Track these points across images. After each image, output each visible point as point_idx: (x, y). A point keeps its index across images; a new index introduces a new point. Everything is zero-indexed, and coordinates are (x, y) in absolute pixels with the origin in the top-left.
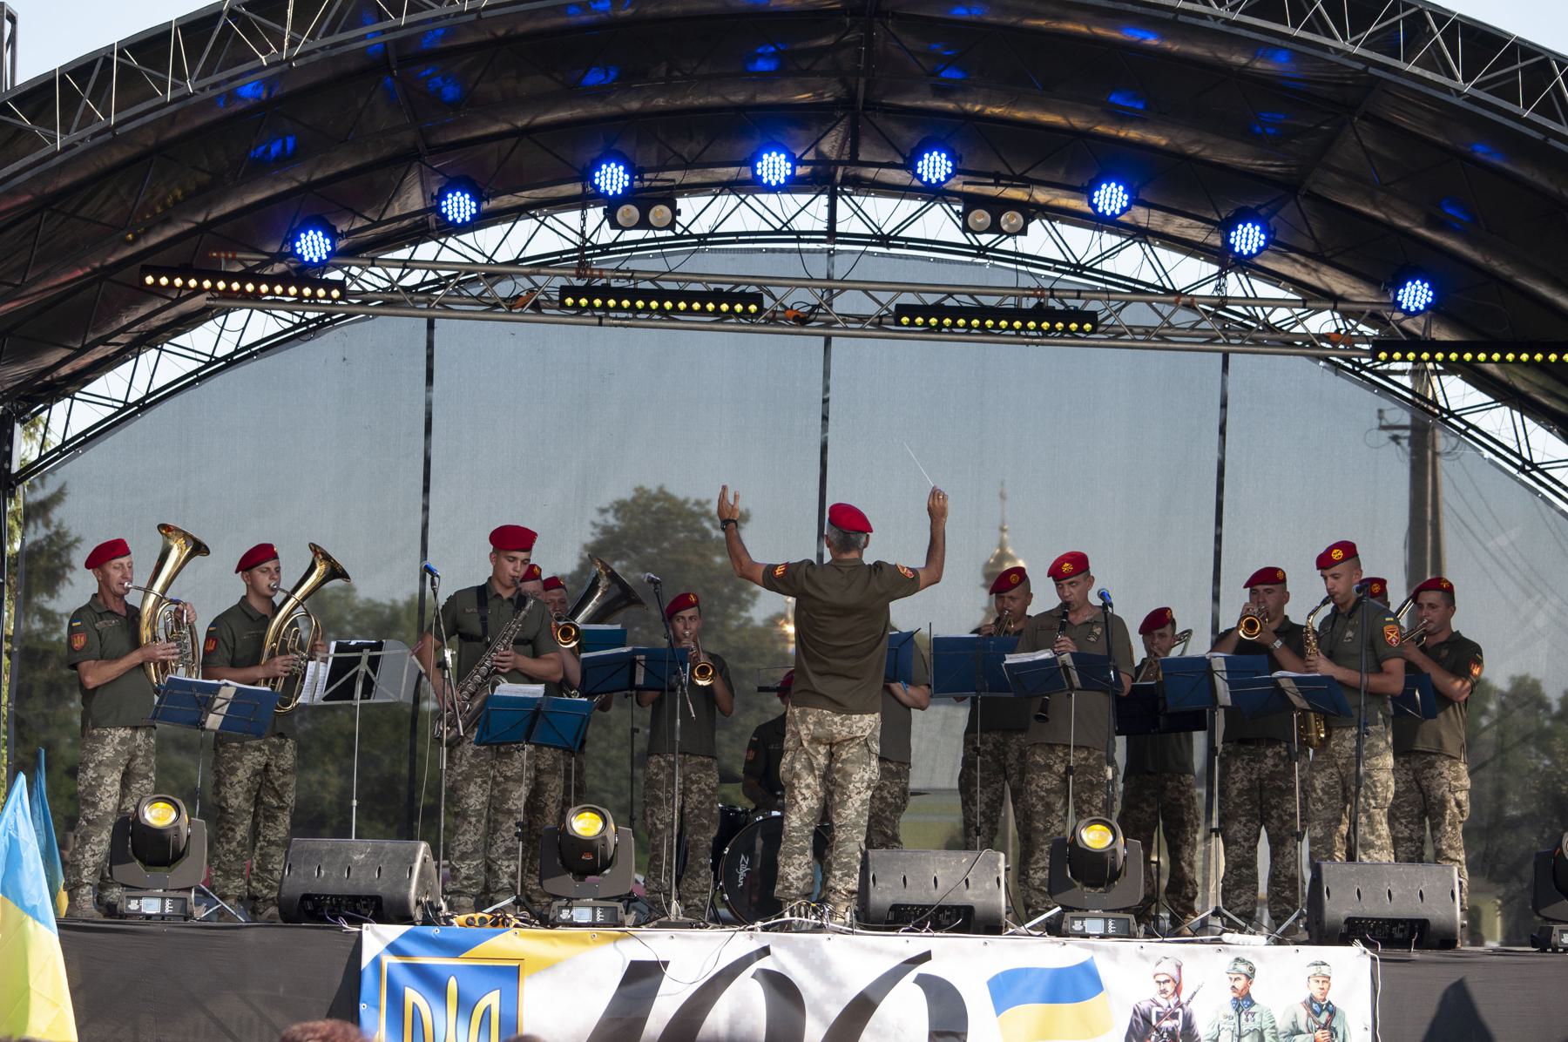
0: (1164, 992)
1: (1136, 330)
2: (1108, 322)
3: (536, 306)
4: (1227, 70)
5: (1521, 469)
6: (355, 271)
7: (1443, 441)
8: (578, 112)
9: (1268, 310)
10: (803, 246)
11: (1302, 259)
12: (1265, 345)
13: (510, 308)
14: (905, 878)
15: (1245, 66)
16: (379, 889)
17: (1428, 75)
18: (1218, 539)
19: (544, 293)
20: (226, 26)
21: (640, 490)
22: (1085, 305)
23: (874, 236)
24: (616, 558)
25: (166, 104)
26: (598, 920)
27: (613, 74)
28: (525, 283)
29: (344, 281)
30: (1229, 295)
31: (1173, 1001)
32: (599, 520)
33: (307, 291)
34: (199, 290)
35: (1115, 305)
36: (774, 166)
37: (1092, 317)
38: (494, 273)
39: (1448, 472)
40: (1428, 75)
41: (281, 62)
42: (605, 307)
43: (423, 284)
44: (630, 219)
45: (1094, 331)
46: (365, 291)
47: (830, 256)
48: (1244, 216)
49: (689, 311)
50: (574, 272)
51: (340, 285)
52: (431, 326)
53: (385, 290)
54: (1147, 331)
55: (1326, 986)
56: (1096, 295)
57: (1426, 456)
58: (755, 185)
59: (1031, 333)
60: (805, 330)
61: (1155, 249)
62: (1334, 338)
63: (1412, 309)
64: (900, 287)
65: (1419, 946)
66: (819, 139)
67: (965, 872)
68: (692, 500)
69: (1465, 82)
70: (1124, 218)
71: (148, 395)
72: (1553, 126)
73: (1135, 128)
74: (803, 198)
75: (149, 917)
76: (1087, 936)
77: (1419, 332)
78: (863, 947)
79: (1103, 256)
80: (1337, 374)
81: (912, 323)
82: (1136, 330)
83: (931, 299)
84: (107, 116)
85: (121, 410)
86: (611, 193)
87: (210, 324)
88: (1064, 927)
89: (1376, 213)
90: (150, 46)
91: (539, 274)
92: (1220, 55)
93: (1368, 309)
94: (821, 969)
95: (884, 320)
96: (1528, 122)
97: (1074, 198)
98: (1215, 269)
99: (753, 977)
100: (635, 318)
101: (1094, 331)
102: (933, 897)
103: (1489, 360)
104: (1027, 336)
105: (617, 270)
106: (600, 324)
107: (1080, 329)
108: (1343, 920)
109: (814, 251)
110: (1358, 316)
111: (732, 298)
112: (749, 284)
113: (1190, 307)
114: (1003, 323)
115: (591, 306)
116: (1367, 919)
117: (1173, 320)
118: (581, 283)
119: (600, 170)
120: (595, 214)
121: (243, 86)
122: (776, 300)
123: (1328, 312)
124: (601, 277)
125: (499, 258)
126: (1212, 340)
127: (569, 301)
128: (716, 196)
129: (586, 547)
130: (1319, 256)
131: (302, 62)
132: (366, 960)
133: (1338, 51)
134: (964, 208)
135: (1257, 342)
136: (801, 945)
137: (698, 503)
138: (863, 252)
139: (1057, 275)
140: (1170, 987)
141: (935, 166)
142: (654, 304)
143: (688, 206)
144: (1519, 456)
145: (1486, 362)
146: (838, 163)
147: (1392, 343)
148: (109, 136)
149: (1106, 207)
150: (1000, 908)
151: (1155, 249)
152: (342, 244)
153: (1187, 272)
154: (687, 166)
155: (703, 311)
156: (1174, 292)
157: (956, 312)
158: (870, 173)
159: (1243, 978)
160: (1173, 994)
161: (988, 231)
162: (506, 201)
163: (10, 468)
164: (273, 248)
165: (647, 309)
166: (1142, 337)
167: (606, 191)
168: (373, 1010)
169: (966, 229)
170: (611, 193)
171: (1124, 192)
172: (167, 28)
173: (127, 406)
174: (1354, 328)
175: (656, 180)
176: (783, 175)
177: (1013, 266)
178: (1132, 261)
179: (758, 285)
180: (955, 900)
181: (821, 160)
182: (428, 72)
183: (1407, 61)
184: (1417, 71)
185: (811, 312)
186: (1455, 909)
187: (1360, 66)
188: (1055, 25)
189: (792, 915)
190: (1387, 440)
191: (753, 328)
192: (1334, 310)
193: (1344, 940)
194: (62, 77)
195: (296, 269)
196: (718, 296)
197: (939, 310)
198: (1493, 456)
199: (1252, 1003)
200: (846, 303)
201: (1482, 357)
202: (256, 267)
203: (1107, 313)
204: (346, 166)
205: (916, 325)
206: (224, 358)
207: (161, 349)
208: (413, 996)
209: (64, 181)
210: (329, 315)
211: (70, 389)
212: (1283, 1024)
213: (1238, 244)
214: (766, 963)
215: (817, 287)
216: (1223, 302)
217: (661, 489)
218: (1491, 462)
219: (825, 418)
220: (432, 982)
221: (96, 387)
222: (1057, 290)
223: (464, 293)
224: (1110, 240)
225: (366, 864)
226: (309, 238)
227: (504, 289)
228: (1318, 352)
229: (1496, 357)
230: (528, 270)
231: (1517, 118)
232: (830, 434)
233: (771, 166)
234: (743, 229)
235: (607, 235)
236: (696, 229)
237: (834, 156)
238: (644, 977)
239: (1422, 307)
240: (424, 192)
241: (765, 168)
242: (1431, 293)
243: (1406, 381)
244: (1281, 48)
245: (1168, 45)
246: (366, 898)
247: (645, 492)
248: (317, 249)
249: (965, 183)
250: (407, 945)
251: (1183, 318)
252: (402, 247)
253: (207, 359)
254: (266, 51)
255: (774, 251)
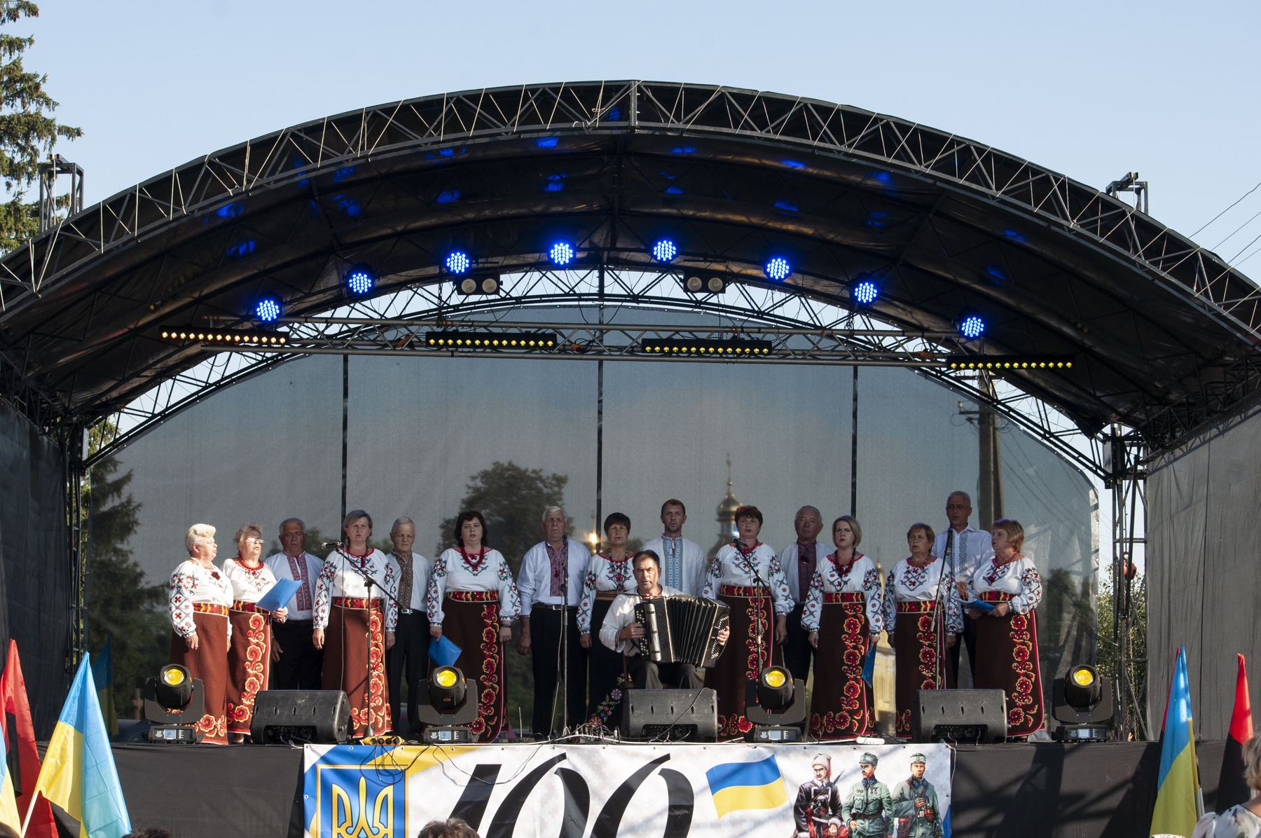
0: (819, 776)
1: (797, 352)
2: (779, 347)
3: (411, 345)
4: (850, 187)
5: (1044, 437)
6: (296, 325)
7: (999, 422)
8: (433, 221)
9: (881, 338)
10: (581, 303)
11: (902, 306)
12: (880, 361)
13: (395, 347)
14: (672, 708)
15: (860, 183)
16: (314, 722)
17: (974, 186)
18: (854, 485)
19: (416, 337)
20: (207, 172)
21: (497, 464)
22: (763, 337)
23: (629, 295)
24: (484, 508)
25: (169, 222)
26: (455, 738)
27: (456, 195)
28: (404, 331)
29: (289, 333)
30: (855, 328)
31: (826, 781)
32: (471, 484)
33: (264, 339)
34: (196, 341)
35: (782, 337)
36: (562, 252)
37: (768, 344)
38: (386, 324)
39: (1004, 440)
40: (974, 186)
41: (242, 193)
42: (455, 345)
43: (340, 333)
44: (471, 288)
45: (769, 353)
46: (301, 339)
47: (601, 309)
48: (864, 278)
49: (509, 346)
50: (434, 323)
51: (285, 335)
52: (346, 360)
53: (315, 337)
54: (804, 353)
55: (922, 769)
56: (771, 330)
57: (989, 430)
58: (549, 265)
59: (729, 356)
60: (585, 357)
61: (809, 301)
62: (922, 355)
63: (971, 336)
64: (644, 328)
65: (982, 741)
66: (591, 234)
67: (691, 702)
68: (530, 470)
69: (997, 190)
70: (787, 281)
71: (167, 409)
72: (1053, 218)
73: (793, 224)
74: (582, 273)
75: (169, 742)
76: (770, 742)
77: (977, 351)
78: (625, 752)
79: (775, 306)
80: (926, 378)
81: (653, 351)
82: (797, 352)
83: (665, 335)
84: (132, 229)
85: (150, 419)
86: (457, 272)
87: (204, 363)
88: (755, 736)
89: (947, 275)
90: (159, 186)
91: (412, 325)
92: (844, 176)
93: (944, 336)
94: (598, 768)
95: (635, 349)
96: (1037, 215)
97: (756, 269)
98: (846, 312)
99: (556, 773)
100: (475, 351)
101: (769, 353)
102: (671, 719)
103: (1020, 367)
104: (727, 358)
105: (463, 321)
106: (452, 356)
107: (761, 352)
108: (933, 727)
109: (591, 306)
110: (938, 341)
111: (536, 337)
112: (548, 328)
113: (831, 337)
114: (711, 350)
115: (446, 344)
116: (949, 726)
117: (820, 346)
118: (440, 330)
119: (450, 257)
120: (448, 287)
121: (221, 208)
122: (565, 338)
123: (920, 339)
124: (452, 326)
125: (388, 315)
126: (845, 358)
127: (432, 341)
128: (527, 272)
129: (464, 502)
130: (913, 303)
131: (256, 192)
132: (307, 767)
133: (917, 172)
134: (685, 277)
135: (875, 359)
136: (586, 752)
137: (534, 471)
138: (621, 306)
139: (746, 318)
140: (823, 773)
141: (665, 250)
142: (487, 342)
143: (508, 280)
144: (1042, 428)
145: (1018, 368)
146: (604, 249)
147: (962, 356)
148: (134, 243)
149: (775, 274)
150: (714, 725)
151: (809, 301)
152: (288, 309)
153: (829, 314)
154: (506, 253)
155: (518, 346)
156: (822, 328)
157: (680, 343)
158: (624, 255)
159: (870, 766)
160: (825, 777)
161: (701, 291)
162: (391, 279)
163: (81, 457)
164: (244, 314)
165: (482, 345)
166: (862, 358)
167: (455, 271)
168: (312, 799)
169: (686, 290)
170: (457, 272)
171: (786, 264)
172: (170, 174)
173: (154, 416)
174: (935, 348)
175: (486, 263)
176: (568, 258)
177: (717, 313)
178: (794, 309)
179: (553, 329)
180: (684, 721)
181: (593, 247)
182: (338, 198)
183: (961, 177)
184: (967, 184)
185: (588, 345)
186: (1003, 717)
187: (931, 181)
188: (738, 159)
189: (580, 733)
190: (964, 420)
191: (551, 356)
192: (922, 337)
193: (934, 739)
194: (104, 207)
195: (258, 326)
196: (527, 336)
197: (670, 342)
198: (1025, 429)
199: (876, 781)
200: (612, 339)
201: (1016, 365)
202: (233, 325)
203: (778, 342)
204: (288, 258)
205: (655, 352)
206: (214, 384)
207: (175, 379)
208: (337, 789)
209: (109, 273)
210: (281, 354)
211: (118, 406)
212: (894, 794)
213: (860, 296)
214: (564, 764)
215: (591, 329)
216: (852, 333)
217: (510, 463)
218: (1025, 432)
219: (600, 412)
220: (350, 780)
221: (135, 404)
222: (746, 328)
223: (365, 338)
224: (779, 296)
225: (305, 706)
226: (265, 305)
227: (390, 335)
228: (913, 364)
229: (1025, 365)
230: (405, 322)
231: (1031, 213)
232: (603, 423)
233: (560, 252)
234: (545, 293)
235: (456, 299)
236: (514, 294)
237: (601, 245)
238: (485, 775)
239: (977, 334)
240: (339, 274)
241: (556, 254)
242: (982, 325)
243: (975, 384)
244: (884, 171)
245: (810, 170)
246: (307, 727)
247: (500, 465)
248: (270, 312)
249: (685, 261)
250: (332, 758)
251: (826, 344)
252: (326, 310)
253: (204, 385)
254: (232, 186)
255: (565, 306)
